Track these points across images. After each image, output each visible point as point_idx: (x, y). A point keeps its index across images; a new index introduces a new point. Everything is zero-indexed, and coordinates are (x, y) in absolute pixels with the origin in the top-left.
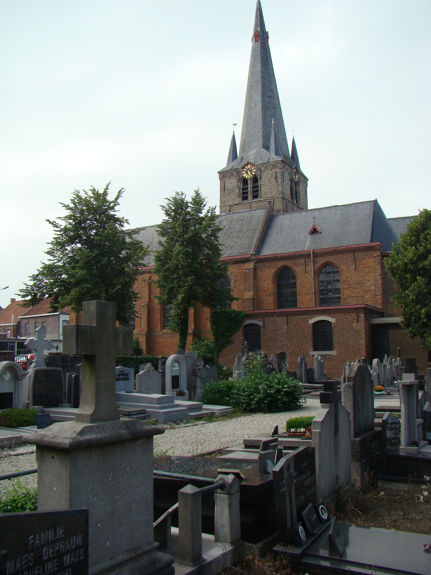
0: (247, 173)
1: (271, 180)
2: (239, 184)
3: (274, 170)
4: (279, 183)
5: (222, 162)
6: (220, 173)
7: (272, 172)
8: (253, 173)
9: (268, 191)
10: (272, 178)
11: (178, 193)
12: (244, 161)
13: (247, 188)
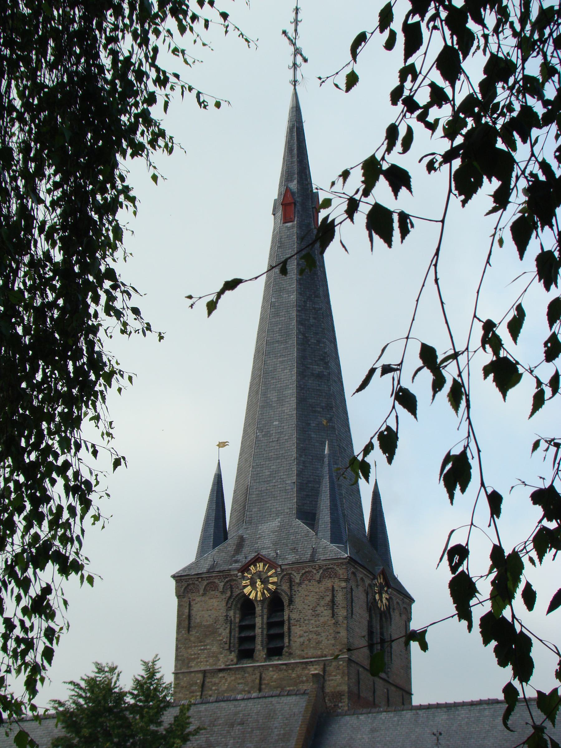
0: (253, 584)
1: (320, 609)
2: (231, 613)
3: (328, 583)
4: (340, 618)
5: (184, 551)
6: (178, 578)
7: (322, 589)
8: (270, 586)
9: (309, 640)
10: (322, 603)
11: (100, 670)
12: (246, 550)
13: (252, 627)
